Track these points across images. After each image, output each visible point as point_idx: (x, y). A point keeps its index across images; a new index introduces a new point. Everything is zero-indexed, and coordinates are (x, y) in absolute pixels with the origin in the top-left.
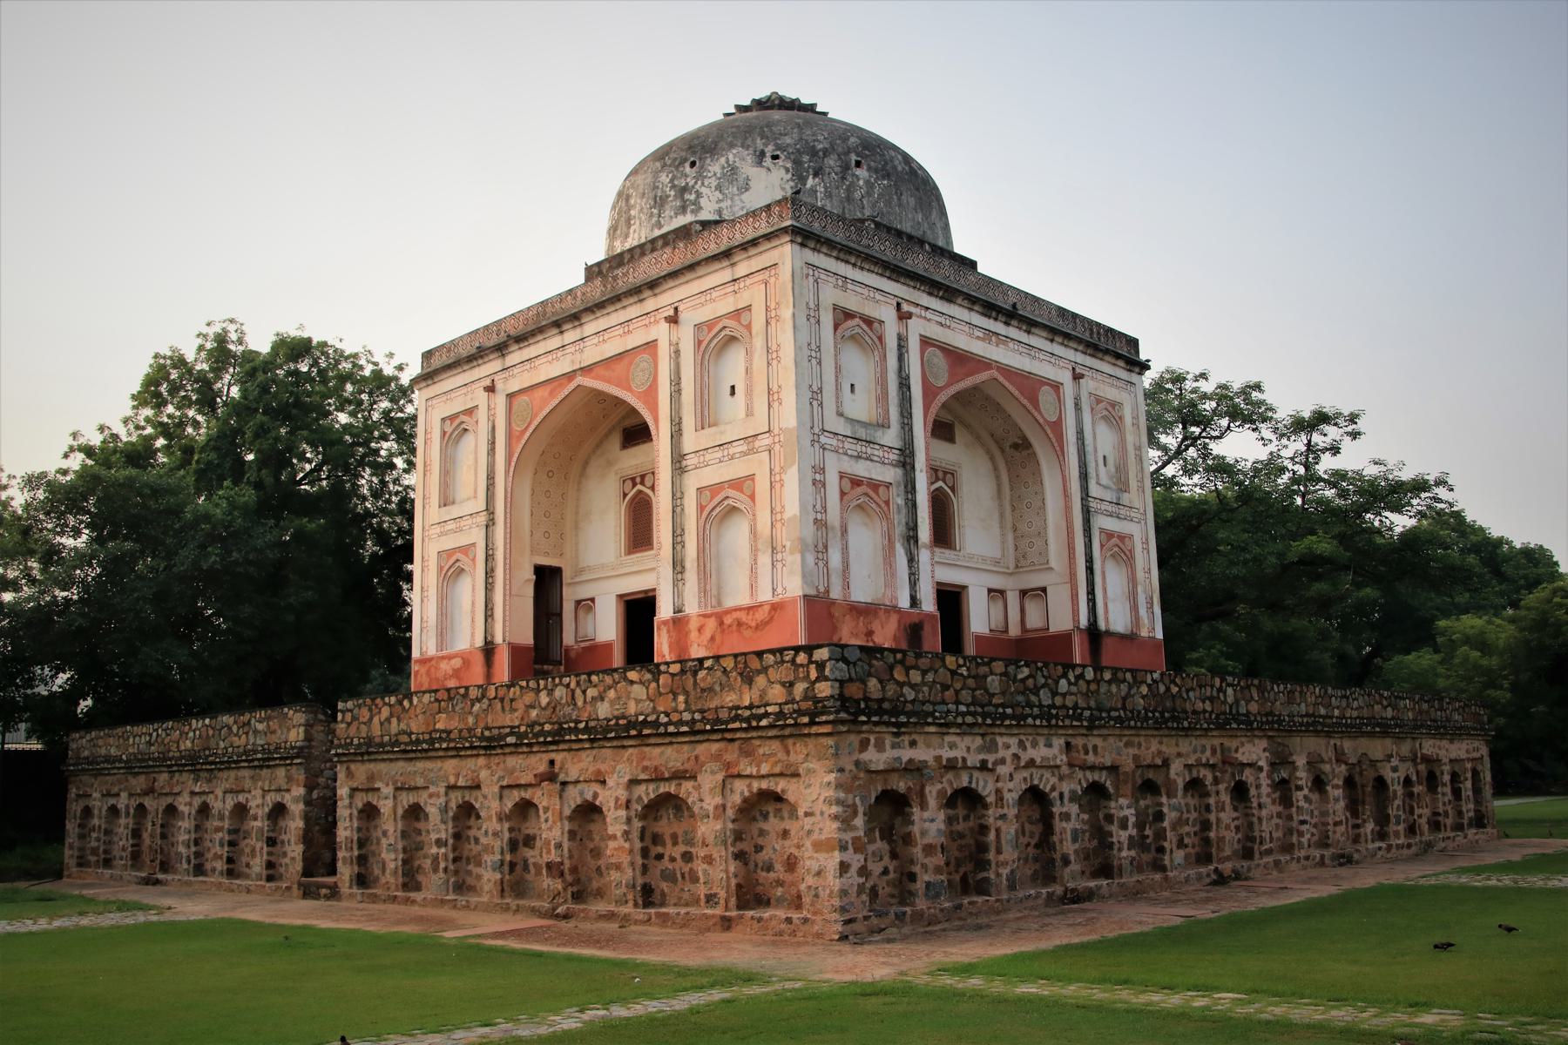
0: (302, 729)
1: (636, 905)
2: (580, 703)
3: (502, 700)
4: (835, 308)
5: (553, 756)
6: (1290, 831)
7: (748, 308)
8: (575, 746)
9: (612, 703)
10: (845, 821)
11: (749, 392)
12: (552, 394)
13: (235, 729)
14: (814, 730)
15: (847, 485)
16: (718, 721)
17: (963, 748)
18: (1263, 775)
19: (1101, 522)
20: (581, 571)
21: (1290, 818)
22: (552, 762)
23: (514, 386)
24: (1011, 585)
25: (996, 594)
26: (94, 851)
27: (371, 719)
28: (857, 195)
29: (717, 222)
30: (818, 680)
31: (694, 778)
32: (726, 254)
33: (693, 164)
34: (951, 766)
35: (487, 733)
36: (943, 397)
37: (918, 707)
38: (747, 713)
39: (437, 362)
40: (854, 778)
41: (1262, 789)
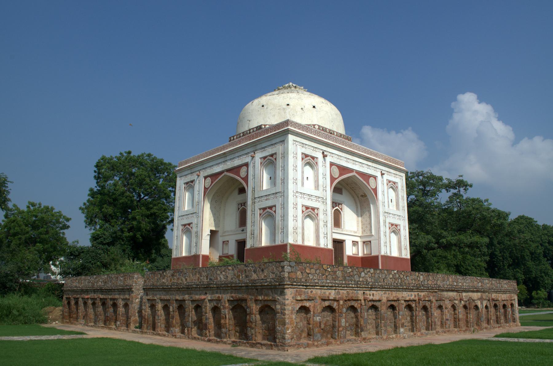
4: (302, 153)
15: (304, 209)
25: (355, 243)
36: (336, 181)
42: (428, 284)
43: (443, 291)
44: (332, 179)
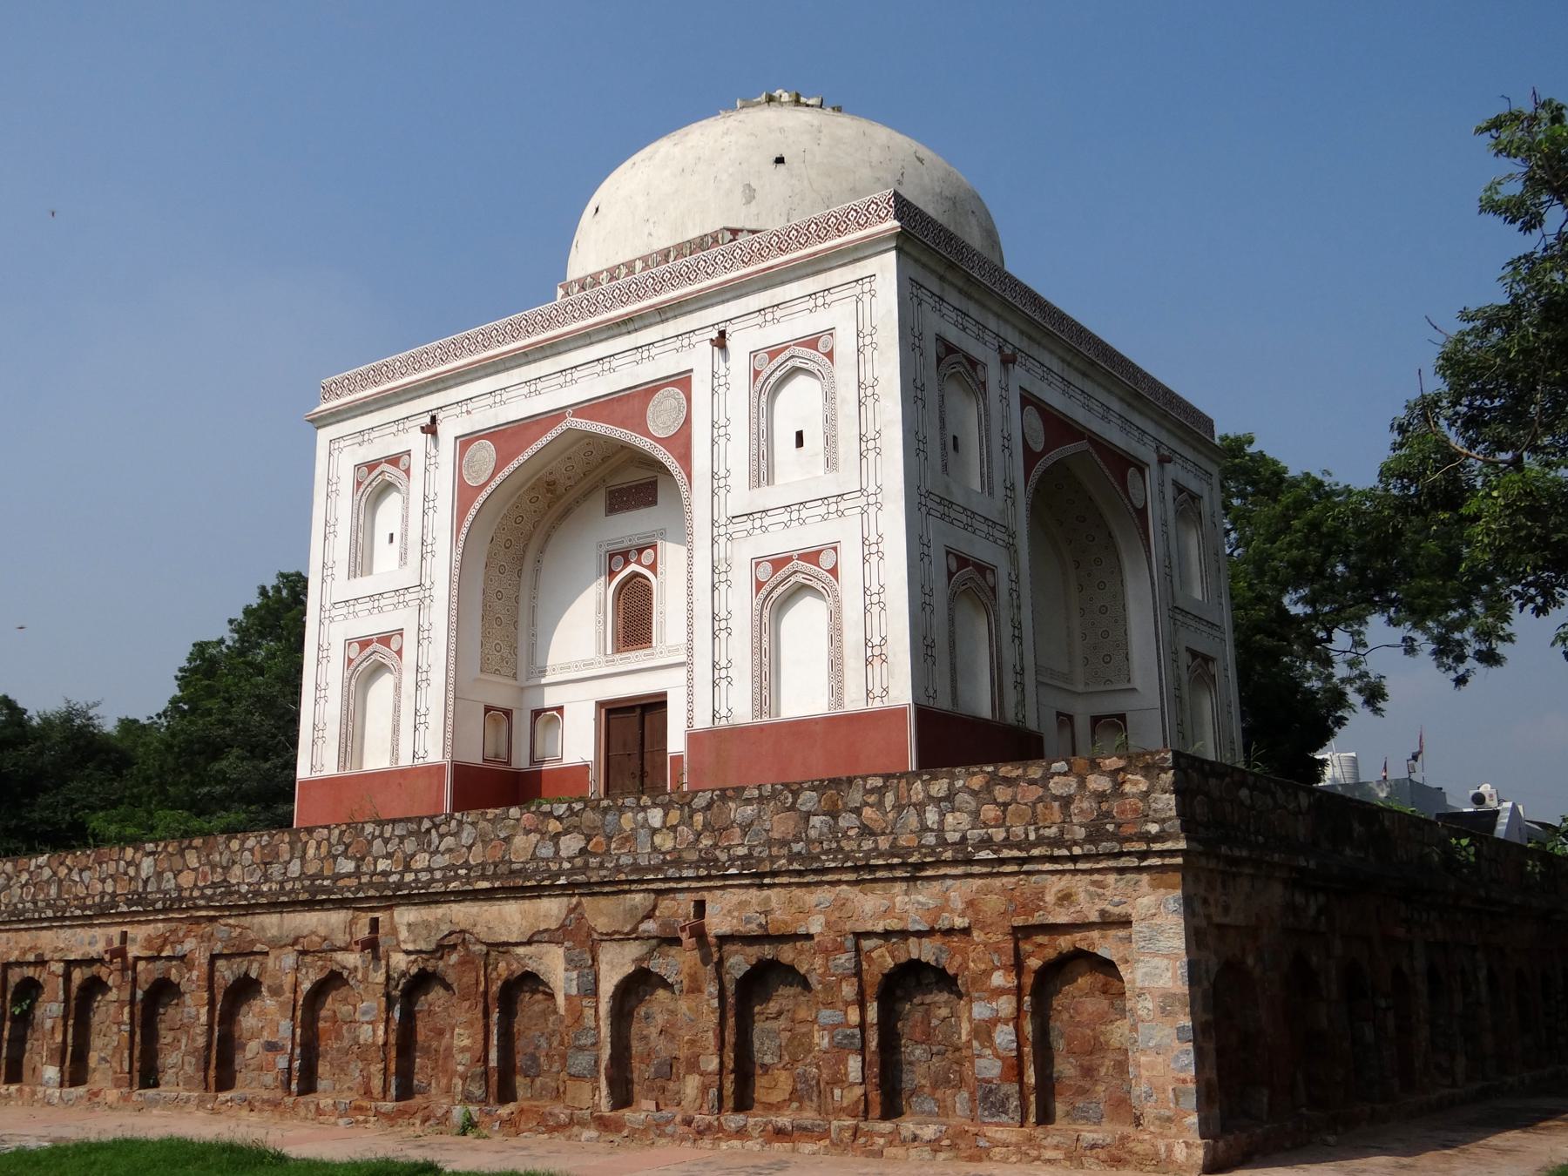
18: (1479, 956)
42: (179, 888)
43: (250, 909)
44: (1030, 458)
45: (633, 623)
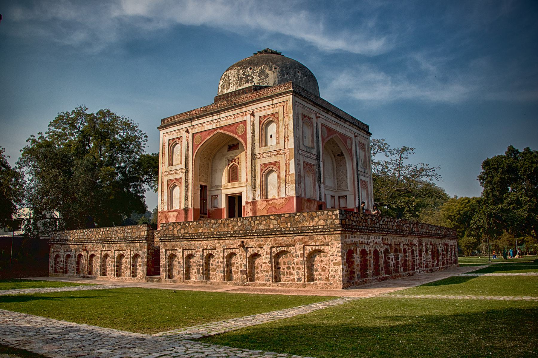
0: (146, 232)
1: (273, 282)
2: (253, 225)
3: (224, 224)
5: (243, 240)
6: (421, 263)
7: (278, 113)
8: (251, 237)
9: (264, 225)
10: (343, 259)
11: (278, 137)
12: (209, 134)
13: (119, 231)
14: (335, 232)
16: (302, 230)
17: (363, 238)
19: (361, 178)
20: (213, 187)
21: (421, 259)
22: (243, 242)
23: (196, 131)
24: (337, 195)
25: (333, 197)
26: (61, 268)
27: (173, 229)
28: (298, 81)
29: (266, 87)
30: (335, 219)
31: (294, 246)
32: (271, 97)
33: (250, 69)
34: (362, 243)
35: (218, 233)
36: (326, 141)
37: (355, 227)
38: (312, 228)
39: (166, 122)
40: (344, 245)
41: (417, 253)
45: (234, 176)
